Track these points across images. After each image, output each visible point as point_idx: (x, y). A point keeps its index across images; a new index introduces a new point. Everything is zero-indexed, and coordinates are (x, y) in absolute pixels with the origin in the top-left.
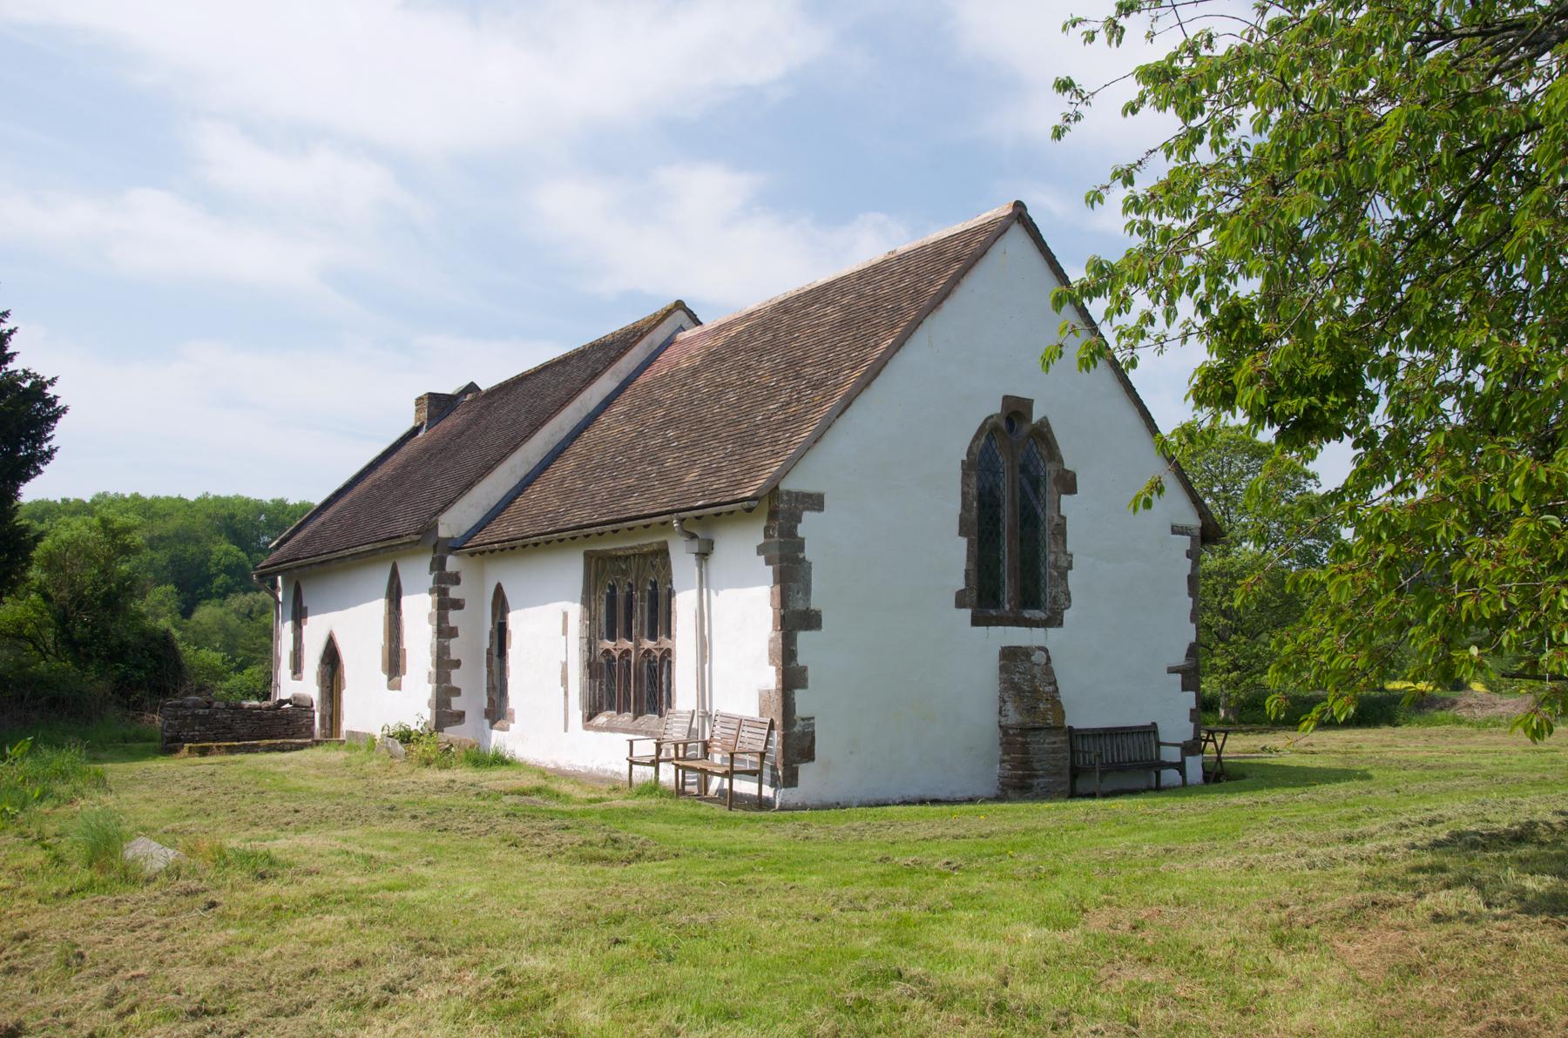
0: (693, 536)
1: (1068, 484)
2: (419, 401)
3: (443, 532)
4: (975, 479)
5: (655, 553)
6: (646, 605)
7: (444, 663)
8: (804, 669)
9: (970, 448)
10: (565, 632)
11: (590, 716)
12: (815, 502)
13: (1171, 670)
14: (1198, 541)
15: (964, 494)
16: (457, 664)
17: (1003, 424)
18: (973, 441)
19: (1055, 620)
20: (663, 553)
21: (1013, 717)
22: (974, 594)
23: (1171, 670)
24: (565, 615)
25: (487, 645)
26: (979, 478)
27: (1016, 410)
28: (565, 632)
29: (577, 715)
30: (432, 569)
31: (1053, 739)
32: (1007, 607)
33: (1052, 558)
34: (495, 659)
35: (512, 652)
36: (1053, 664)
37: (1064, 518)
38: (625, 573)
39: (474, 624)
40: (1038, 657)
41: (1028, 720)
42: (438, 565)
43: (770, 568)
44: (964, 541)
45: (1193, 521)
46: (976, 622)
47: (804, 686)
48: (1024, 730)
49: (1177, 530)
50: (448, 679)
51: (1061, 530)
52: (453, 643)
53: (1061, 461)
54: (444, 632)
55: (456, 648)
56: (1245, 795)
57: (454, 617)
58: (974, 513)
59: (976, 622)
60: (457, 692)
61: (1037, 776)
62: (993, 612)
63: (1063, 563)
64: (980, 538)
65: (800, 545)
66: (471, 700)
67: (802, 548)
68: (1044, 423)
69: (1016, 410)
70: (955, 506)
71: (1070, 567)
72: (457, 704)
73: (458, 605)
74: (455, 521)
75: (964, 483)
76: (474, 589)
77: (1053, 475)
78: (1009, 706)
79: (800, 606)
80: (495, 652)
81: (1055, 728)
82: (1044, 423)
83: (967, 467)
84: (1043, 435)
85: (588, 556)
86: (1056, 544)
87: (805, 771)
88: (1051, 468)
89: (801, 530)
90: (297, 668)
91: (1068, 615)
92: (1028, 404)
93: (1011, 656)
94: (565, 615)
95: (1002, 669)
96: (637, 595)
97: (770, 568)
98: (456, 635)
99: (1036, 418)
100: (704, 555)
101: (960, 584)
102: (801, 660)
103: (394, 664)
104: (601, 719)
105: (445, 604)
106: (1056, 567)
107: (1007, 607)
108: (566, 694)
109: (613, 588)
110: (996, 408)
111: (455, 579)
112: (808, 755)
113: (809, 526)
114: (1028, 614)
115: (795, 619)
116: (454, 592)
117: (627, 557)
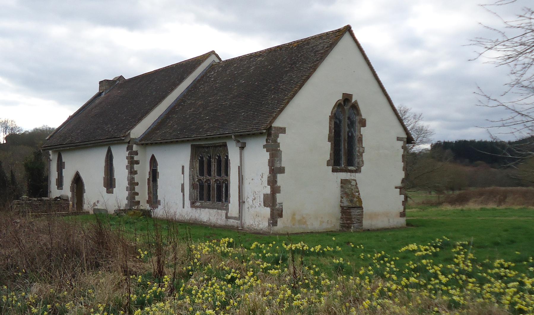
0: (238, 142)
1: (363, 123)
3: (132, 136)
5: (220, 146)
6: (216, 164)
7: (132, 184)
8: (280, 187)
9: (332, 111)
10: (183, 173)
12: (283, 130)
14: (406, 142)
15: (330, 127)
16: (137, 184)
17: (343, 103)
19: (358, 171)
20: (225, 146)
21: (346, 203)
23: (396, 188)
24: (183, 167)
25: (147, 176)
27: (347, 98)
28: (183, 173)
29: (188, 202)
30: (127, 150)
32: (343, 166)
33: (357, 149)
35: (160, 181)
36: (358, 186)
37: (362, 135)
38: (208, 153)
40: (353, 183)
42: (129, 148)
43: (268, 153)
45: (404, 136)
46: (334, 171)
47: (279, 192)
48: (349, 208)
49: (399, 139)
50: (134, 189)
51: (360, 140)
53: (361, 116)
54: (132, 172)
55: (137, 178)
59: (334, 171)
60: (137, 194)
62: (338, 167)
63: (361, 151)
66: (143, 196)
67: (279, 147)
68: (356, 102)
69: (347, 98)
70: (327, 132)
71: (363, 152)
72: (137, 198)
73: (137, 162)
74: (138, 131)
75: (330, 124)
78: (344, 200)
82: (356, 102)
83: (331, 118)
84: (355, 107)
85: (192, 145)
86: (359, 143)
87: (280, 221)
88: (357, 118)
89: (279, 140)
90: (60, 184)
91: (362, 168)
92: (350, 96)
94: (183, 167)
95: (342, 187)
96: (213, 160)
97: (268, 153)
98: (137, 174)
99: (353, 101)
100: (242, 148)
101: (328, 158)
102: (279, 184)
103: (110, 183)
104: (198, 204)
105: (132, 162)
106: (359, 152)
107: (343, 166)
108: (184, 195)
109: (202, 158)
110: (340, 97)
111: (136, 153)
112: (281, 216)
113: (281, 139)
114: (350, 168)
115: (275, 170)
116: (136, 158)
117: (208, 147)
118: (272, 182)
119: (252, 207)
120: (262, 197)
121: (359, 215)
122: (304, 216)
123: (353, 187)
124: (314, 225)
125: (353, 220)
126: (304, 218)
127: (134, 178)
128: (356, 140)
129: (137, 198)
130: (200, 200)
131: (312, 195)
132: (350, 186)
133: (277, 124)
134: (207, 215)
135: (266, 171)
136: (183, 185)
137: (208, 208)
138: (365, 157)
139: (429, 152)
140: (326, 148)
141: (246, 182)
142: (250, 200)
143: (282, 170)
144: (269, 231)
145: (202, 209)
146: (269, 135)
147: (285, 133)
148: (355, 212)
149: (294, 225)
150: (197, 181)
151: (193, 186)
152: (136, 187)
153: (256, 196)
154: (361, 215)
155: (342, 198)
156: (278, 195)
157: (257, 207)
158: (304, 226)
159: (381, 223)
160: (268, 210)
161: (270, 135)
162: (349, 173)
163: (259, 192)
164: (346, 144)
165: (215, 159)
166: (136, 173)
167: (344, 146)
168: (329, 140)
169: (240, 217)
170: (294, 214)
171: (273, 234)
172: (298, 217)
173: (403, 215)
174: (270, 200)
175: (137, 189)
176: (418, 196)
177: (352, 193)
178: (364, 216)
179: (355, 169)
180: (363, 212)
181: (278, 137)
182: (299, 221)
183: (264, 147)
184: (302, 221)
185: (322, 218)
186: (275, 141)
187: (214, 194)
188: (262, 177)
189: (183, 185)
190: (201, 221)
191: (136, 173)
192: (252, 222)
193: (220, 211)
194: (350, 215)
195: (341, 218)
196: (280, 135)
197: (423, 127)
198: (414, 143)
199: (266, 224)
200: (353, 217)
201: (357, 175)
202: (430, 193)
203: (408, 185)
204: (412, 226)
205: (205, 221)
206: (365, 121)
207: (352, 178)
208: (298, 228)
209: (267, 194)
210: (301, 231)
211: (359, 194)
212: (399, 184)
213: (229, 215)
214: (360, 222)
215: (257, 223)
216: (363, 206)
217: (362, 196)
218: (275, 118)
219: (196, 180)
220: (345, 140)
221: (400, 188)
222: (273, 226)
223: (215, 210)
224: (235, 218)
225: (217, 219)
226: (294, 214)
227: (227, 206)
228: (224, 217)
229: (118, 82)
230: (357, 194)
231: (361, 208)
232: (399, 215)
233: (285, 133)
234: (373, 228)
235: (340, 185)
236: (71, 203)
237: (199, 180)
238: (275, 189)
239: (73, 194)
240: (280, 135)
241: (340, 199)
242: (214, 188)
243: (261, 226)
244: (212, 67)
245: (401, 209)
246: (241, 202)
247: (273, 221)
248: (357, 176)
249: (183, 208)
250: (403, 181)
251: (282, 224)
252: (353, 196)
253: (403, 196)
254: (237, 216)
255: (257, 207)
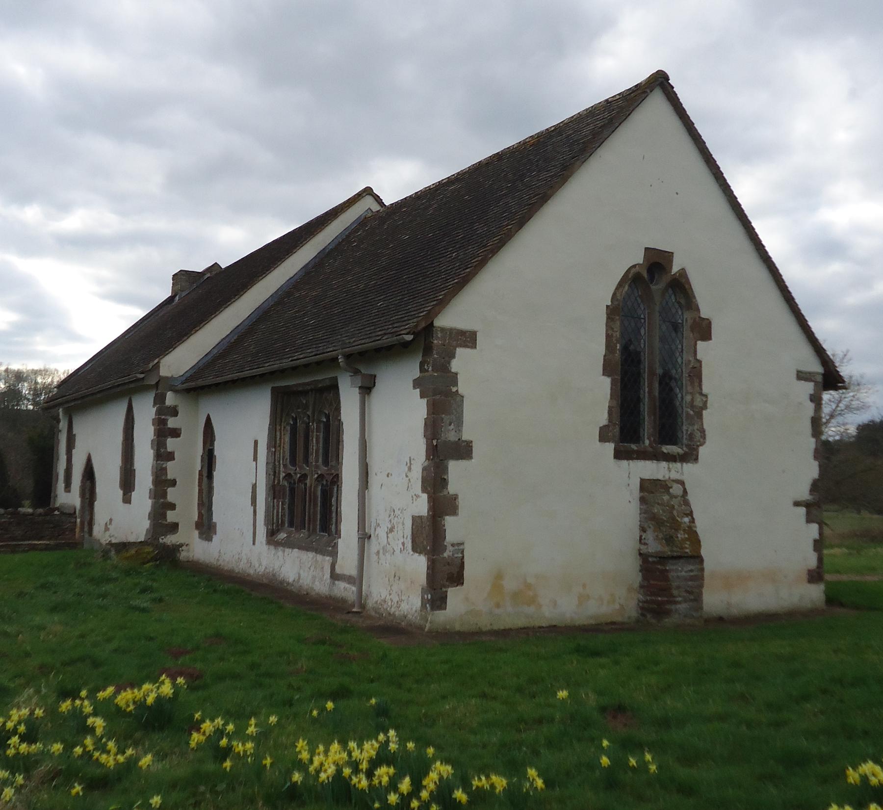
0: (356, 372)
1: (704, 330)
2: (175, 276)
3: (164, 372)
4: (618, 323)
7: (162, 483)
8: (455, 497)
9: (614, 295)
10: (255, 459)
11: (271, 534)
12: (469, 339)
13: (797, 504)
15: (608, 337)
16: (173, 483)
17: (645, 274)
18: (617, 289)
19: (690, 456)
20: (334, 387)
21: (654, 546)
22: (617, 429)
23: (797, 504)
24: (256, 442)
25: (198, 467)
26: (622, 322)
27: (657, 263)
28: (255, 459)
30: (155, 404)
31: (691, 567)
32: (647, 442)
33: (688, 398)
34: (205, 479)
36: (690, 497)
37: (700, 362)
39: (187, 451)
40: (676, 490)
41: (667, 551)
42: (159, 400)
43: (425, 401)
44: (607, 381)
45: (816, 367)
46: (619, 455)
48: (663, 559)
49: (802, 376)
50: (164, 495)
51: (696, 374)
52: (170, 465)
53: (698, 310)
54: (162, 455)
55: (172, 469)
56: (344, 417)
57: (171, 444)
58: (618, 354)
59: (619, 455)
60: (172, 507)
61: (676, 603)
62: (634, 447)
63: (698, 402)
64: (622, 379)
65: (453, 379)
66: (185, 512)
67: (456, 384)
68: (683, 273)
69: (657, 263)
70: (599, 347)
71: (705, 406)
72: (171, 516)
73: (176, 433)
76: (188, 421)
77: (690, 322)
78: (650, 536)
79: (452, 437)
80: (205, 474)
81: (692, 557)
82: (683, 273)
83: (612, 312)
84: (681, 287)
85: (274, 391)
86: (692, 383)
87: (454, 596)
88: (688, 315)
89: (455, 365)
91: (702, 450)
93: (649, 488)
94: (256, 442)
95: (642, 500)
97: (425, 401)
99: (675, 269)
100: (367, 389)
101: (603, 418)
102: (452, 489)
103: (127, 483)
104: (282, 535)
105: (163, 432)
106: (692, 405)
107: (647, 442)
111: (174, 412)
112: (457, 579)
113: (463, 362)
114: (666, 449)
115: (444, 448)
116: (172, 423)
118: (435, 482)
119: (385, 550)
120: (409, 524)
121: (692, 579)
122: (529, 580)
123: (674, 502)
124: (561, 606)
125: (675, 592)
126: (529, 586)
127: (165, 469)
128: (685, 375)
129: (171, 516)
130: (291, 524)
131: (551, 525)
132: (666, 498)
133: (451, 318)
134: (297, 567)
135: (417, 449)
136: (254, 487)
137: (300, 548)
138: (709, 418)
139: (852, 440)
140: (598, 394)
141: (375, 480)
142: (382, 532)
143: (464, 450)
144: (422, 622)
145: (288, 550)
146: (428, 350)
147: (474, 346)
148: (679, 571)
149: (498, 605)
150: (284, 478)
151: (274, 491)
152: (170, 490)
153: (395, 521)
154: (699, 578)
155: (643, 530)
156: (450, 523)
157: (398, 551)
158: (531, 610)
159: (754, 599)
160: (420, 564)
161: (430, 351)
162: (664, 464)
163: (402, 510)
164: (656, 385)
165: (319, 422)
166: (170, 456)
167: (649, 391)
168: (607, 370)
169: (357, 580)
170: (499, 577)
171: (430, 631)
172: (510, 585)
173: (815, 576)
174: (429, 535)
175: (172, 495)
176: (845, 521)
177: (674, 518)
178: (707, 581)
179: (680, 451)
180: (702, 570)
181: (452, 356)
182: (516, 596)
183: (417, 383)
184: (525, 595)
185: (584, 586)
186: (444, 368)
187: (315, 513)
188: (410, 469)
189: (254, 487)
190: (282, 582)
191: (170, 456)
192: (384, 594)
193: (319, 557)
194: (666, 579)
195: (641, 587)
196: (460, 351)
197: (851, 377)
198: (845, 388)
199: (417, 602)
200: (674, 584)
201: (688, 467)
202: (859, 512)
203: (821, 501)
204: (842, 605)
205: (291, 580)
206: (710, 323)
207: (674, 475)
208: (511, 616)
209: (421, 517)
210: (520, 622)
211: (693, 521)
212: (804, 494)
213: (338, 570)
214: (696, 598)
215: (396, 599)
216: (703, 552)
217: (701, 526)
218: (442, 304)
219: (282, 475)
220: (652, 373)
221: (807, 505)
222: (433, 609)
223: (311, 555)
224: (349, 579)
225: (314, 577)
226: (499, 577)
227: (335, 546)
228: (327, 575)
229: (208, 275)
230: (686, 520)
231: (698, 559)
232: (805, 576)
233: (474, 346)
234: (735, 611)
235: (637, 493)
236: (78, 520)
237: (288, 476)
238: (442, 504)
239: (82, 502)
240: (460, 351)
241: (637, 533)
242: (315, 493)
243: (405, 608)
244: (362, 222)
245: (812, 561)
246: (364, 537)
247: (436, 596)
248: (687, 471)
249: (254, 544)
250: (815, 486)
251: (459, 605)
252: (676, 525)
253: (815, 527)
254: (353, 572)
255: (398, 551)
